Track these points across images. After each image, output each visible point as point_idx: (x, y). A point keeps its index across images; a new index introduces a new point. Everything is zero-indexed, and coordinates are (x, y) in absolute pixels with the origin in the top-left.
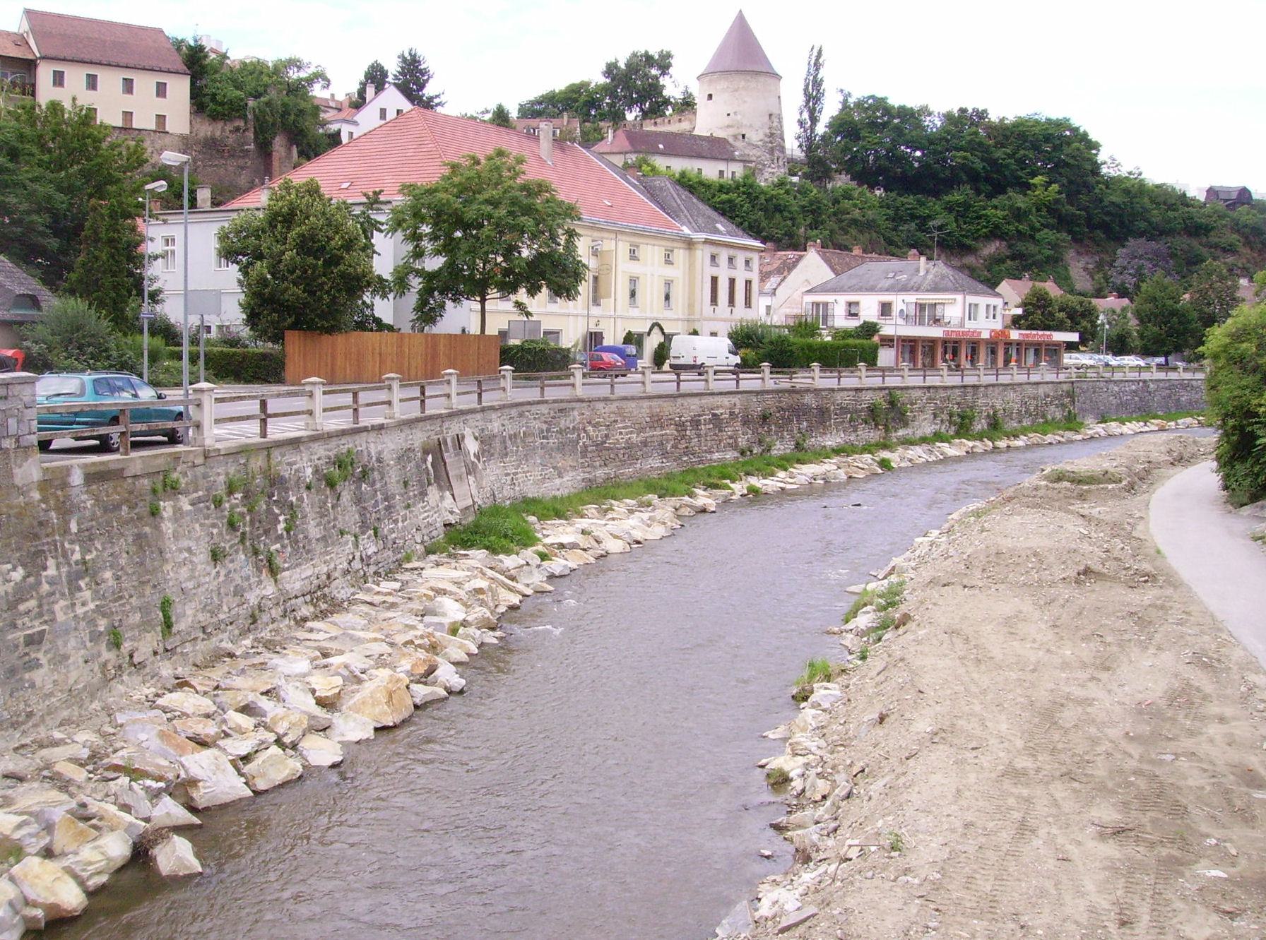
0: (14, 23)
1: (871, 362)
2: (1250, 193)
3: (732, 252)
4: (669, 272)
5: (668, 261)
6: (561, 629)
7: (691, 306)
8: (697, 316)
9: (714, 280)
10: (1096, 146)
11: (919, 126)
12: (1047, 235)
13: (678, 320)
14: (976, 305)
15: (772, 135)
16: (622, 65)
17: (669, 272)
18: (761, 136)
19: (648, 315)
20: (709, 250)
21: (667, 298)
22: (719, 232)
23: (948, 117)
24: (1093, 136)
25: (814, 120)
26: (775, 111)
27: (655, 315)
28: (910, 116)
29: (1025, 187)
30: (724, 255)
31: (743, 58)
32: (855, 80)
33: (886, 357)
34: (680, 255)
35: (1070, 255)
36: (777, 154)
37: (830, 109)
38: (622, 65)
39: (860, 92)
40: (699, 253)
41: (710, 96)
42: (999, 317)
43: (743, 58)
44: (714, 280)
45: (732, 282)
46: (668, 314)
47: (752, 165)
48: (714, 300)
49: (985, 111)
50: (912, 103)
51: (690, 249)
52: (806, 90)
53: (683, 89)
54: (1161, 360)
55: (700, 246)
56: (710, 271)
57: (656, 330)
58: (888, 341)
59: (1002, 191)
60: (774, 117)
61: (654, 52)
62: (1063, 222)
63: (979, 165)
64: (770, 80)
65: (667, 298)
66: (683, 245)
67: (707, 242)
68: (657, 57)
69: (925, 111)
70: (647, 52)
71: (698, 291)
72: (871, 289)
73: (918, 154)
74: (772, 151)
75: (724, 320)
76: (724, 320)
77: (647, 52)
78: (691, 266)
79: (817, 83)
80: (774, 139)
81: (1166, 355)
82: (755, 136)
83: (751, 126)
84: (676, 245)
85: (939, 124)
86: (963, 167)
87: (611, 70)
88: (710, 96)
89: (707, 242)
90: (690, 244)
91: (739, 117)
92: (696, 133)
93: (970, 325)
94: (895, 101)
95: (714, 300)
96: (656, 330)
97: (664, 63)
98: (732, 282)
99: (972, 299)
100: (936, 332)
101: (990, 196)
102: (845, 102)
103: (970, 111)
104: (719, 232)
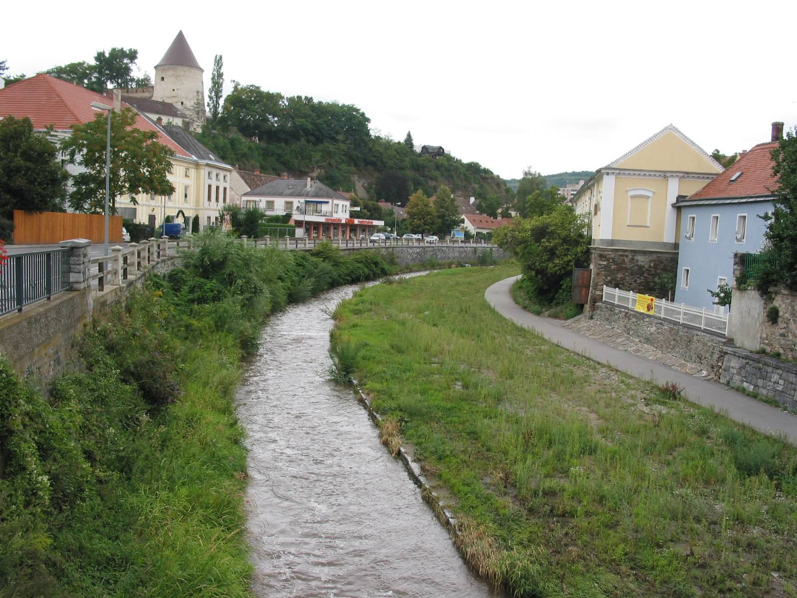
0: (32, 54)
1: (292, 234)
2: (443, 149)
3: (218, 171)
4: (187, 181)
5: (187, 176)
6: (615, 266)
7: (197, 202)
8: (201, 207)
9: (210, 186)
10: (368, 120)
11: (276, 104)
12: (344, 167)
13: (190, 209)
14: (338, 205)
15: (198, 103)
16: (107, 55)
17: (187, 181)
18: (192, 103)
19: (177, 206)
20: (207, 169)
21: (186, 196)
22: (212, 160)
23: (291, 100)
24: (367, 115)
25: (218, 97)
26: (200, 90)
27: (180, 206)
28: (273, 98)
29: (334, 140)
30: (214, 172)
31: (180, 55)
32: (241, 74)
33: (300, 232)
34: (192, 172)
35: (355, 178)
36: (201, 114)
37: (227, 90)
38: (107, 55)
39: (245, 82)
40: (202, 171)
41: (163, 79)
42: (348, 213)
43: (180, 55)
44: (210, 186)
45: (218, 188)
46: (186, 206)
47: (187, 120)
48: (209, 199)
49: (311, 98)
50: (292, 96)
51: (197, 169)
52: (213, 79)
53: (144, 73)
54: (420, 236)
55: (203, 167)
56: (208, 182)
57: (181, 215)
58: (299, 224)
59: (321, 141)
60: (199, 93)
61: (126, 49)
62: (352, 160)
63: (310, 127)
64: (198, 72)
65: (186, 196)
66: (193, 166)
67: (208, 165)
68: (128, 52)
69: (279, 96)
70: (122, 49)
71: (201, 192)
72: (280, 195)
73: (276, 119)
74: (198, 113)
75: (214, 210)
76: (214, 210)
77: (122, 49)
78: (198, 178)
79: (220, 75)
80: (199, 104)
81: (422, 233)
82: (189, 104)
83: (186, 98)
84: (190, 166)
85: (287, 104)
86: (301, 126)
87: (100, 57)
88: (163, 79)
89: (208, 165)
90: (197, 166)
91: (180, 92)
92: (154, 98)
93: (335, 216)
94: (264, 89)
95: (209, 199)
96: (181, 215)
97: (133, 55)
98: (218, 188)
99: (336, 202)
100: (322, 219)
101: (315, 144)
102: (236, 87)
103: (303, 98)
104: (212, 160)
